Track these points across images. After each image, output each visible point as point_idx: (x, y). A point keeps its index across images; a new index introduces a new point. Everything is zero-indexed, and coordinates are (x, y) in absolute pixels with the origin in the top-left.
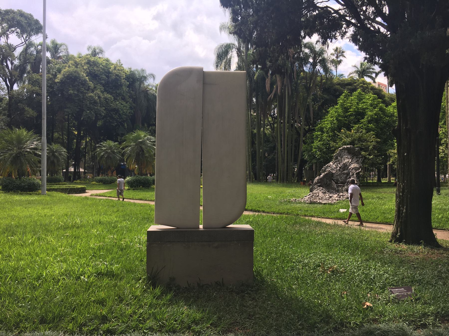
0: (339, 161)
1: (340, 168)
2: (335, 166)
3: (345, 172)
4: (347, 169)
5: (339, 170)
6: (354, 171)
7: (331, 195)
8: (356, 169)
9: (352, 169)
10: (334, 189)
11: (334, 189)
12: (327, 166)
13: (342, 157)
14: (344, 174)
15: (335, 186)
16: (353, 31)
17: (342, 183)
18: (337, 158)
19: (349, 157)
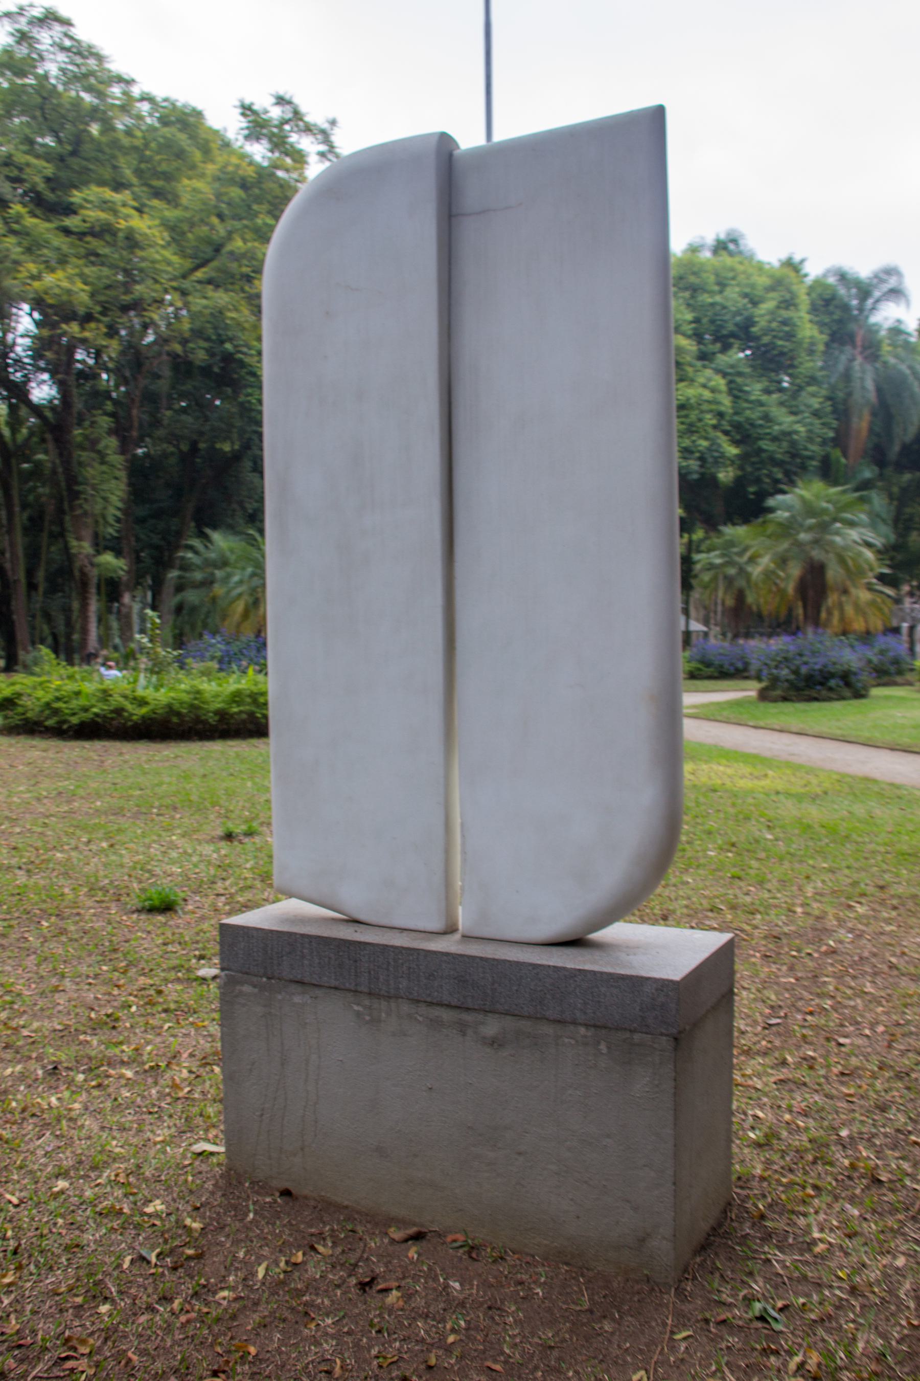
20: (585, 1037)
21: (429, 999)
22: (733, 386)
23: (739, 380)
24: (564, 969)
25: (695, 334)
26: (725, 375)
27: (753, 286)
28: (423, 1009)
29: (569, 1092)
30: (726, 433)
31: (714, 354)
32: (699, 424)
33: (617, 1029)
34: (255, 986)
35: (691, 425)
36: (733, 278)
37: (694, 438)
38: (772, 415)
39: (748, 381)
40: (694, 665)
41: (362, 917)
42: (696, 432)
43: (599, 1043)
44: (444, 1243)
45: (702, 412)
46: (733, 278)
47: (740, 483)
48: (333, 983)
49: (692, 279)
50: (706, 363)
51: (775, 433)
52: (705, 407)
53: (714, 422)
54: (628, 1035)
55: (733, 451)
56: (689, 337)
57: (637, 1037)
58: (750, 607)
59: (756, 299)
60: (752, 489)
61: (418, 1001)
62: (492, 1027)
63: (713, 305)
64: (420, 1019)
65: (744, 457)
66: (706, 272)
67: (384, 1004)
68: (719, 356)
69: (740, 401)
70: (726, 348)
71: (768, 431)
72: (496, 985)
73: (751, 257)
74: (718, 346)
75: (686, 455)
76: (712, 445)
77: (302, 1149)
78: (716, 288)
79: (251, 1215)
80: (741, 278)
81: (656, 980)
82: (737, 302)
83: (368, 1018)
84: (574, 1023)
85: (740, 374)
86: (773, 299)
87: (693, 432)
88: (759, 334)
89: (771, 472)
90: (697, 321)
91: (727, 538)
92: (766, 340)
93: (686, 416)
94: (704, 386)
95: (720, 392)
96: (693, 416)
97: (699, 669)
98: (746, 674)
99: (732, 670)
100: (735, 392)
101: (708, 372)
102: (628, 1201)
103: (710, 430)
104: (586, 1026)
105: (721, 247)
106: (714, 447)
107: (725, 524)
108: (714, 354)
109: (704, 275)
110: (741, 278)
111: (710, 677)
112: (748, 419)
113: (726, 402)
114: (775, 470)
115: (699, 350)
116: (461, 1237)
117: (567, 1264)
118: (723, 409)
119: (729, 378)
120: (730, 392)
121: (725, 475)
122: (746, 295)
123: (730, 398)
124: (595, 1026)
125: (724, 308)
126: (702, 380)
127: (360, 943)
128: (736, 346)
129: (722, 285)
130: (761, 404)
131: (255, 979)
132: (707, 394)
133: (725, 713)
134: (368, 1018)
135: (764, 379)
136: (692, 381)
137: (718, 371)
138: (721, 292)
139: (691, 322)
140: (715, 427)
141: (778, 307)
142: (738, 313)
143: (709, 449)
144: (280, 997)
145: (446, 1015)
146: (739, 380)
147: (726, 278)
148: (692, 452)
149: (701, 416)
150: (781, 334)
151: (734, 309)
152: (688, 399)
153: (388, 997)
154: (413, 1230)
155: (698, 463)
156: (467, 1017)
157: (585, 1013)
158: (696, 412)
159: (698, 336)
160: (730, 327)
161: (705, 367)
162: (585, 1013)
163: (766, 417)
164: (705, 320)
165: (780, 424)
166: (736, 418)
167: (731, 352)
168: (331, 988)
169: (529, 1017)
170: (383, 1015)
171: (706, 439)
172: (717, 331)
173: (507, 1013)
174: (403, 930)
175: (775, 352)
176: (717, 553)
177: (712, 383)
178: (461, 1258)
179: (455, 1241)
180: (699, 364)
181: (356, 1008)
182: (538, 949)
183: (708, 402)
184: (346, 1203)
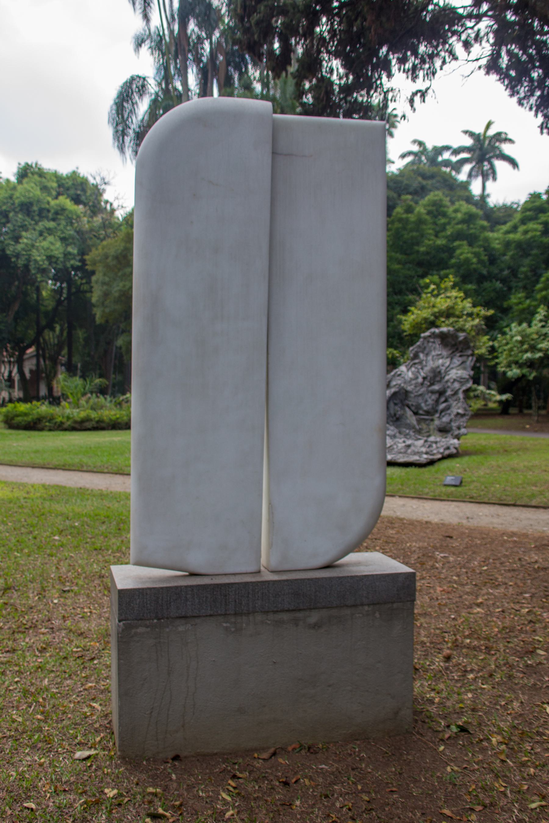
0: (420, 363)
1: (424, 378)
2: (413, 373)
3: (436, 387)
4: (440, 381)
5: (422, 384)
6: (456, 385)
7: (409, 442)
8: (461, 381)
9: (453, 383)
10: (410, 427)
11: (410, 427)
12: (394, 376)
13: (427, 355)
14: (433, 392)
15: (412, 419)
16: (67, 198)
17: (428, 413)
18: (416, 356)
19: (445, 353)
21: (275, 609)
28: (271, 616)
34: (147, 627)
48: (209, 612)
57: (395, 605)
61: (268, 612)
62: (314, 617)
64: (269, 622)
67: (244, 618)
77: (183, 726)
84: (362, 605)
104: (369, 605)
117: (357, 740)
134: (233, 629)
144: (167, 630)
145: (285, 616)
154: (272, 750)
168: (207, 616)
169: (337, 607)
179: (294, 749)
181: (225, 625)
182: (320, 571)
184: (215, 751)
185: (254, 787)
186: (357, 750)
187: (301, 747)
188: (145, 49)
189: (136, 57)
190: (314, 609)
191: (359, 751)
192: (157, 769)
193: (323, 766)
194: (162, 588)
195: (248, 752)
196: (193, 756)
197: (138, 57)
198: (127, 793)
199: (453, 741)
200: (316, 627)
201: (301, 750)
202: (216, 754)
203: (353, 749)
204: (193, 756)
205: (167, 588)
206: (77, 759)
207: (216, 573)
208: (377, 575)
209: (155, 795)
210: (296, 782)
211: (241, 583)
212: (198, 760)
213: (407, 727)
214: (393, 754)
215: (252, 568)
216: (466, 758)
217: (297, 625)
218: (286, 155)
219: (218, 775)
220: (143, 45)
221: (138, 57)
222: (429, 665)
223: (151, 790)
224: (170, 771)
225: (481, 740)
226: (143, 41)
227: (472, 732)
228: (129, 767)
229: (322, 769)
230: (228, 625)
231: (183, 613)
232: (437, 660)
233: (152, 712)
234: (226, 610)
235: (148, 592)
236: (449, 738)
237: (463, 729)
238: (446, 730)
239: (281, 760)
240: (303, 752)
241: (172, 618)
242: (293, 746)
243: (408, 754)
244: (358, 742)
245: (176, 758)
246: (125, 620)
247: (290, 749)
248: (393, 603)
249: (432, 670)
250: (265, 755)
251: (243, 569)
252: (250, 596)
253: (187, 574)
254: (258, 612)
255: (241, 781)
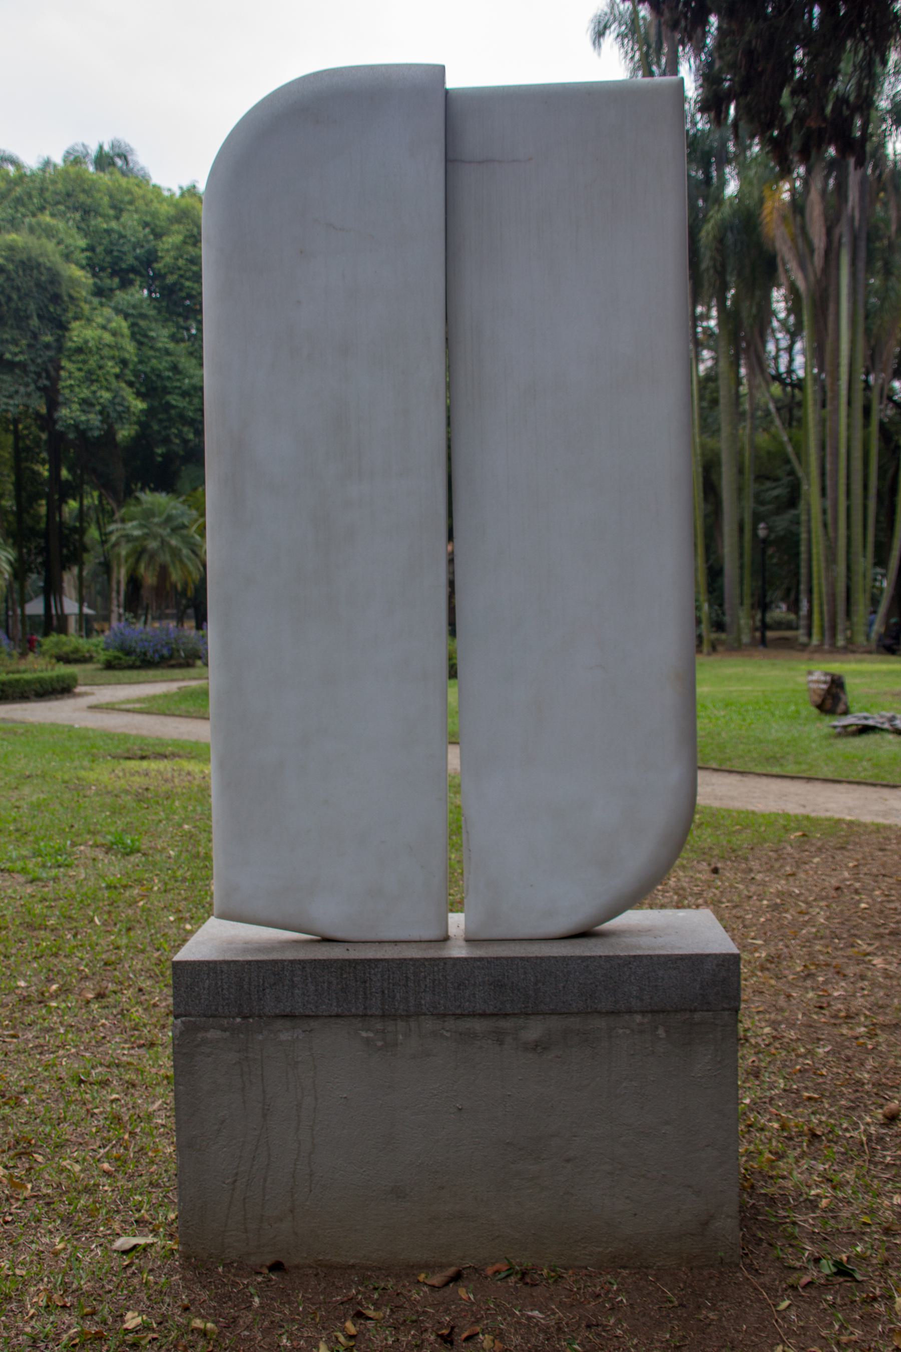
20: (641, 1024)
21: (459, 1011)
22: (136, 329)
23: (142, 323)
24: (618, 957)
25: (88, 265)
26: (126, 316)
27: (155, 215)
28: (451, 1023)
29: (624, 1084)
30: (130, 384)
31: (112, 290)
32: (100, 372)
33: (676, 1011)
34: (224, 1030)
35: (90, 372)
36: (131, 202)
37: (94, 388)
38: (181, 366)
39: (153, 325)
40: (112, 653)
41: (339, 935)
42: (97, 381)
43: (656, 1028)
44: (486, 1277)
45: (102, 358)
46: (131, 202)
47: (143, 440)
48: (335, 1010)
49: (82, 197)
50: (104, 300)
51: (185, 387)
52: (106, 352)
53: (117, 370)
54: (687, 1015)
55: (139, 405)
56: (82, 268)
57: (697, 1016)
58: (174, 586)
59: (158, 230)
60: (159, 451)
61: (445, 1015)
62: (534, 1030)
63: (108, 232)
64: (448, 1035)
65: (150, 412)
66: (99, 191)
67: (401, 1025)
68: (118, 292)
69: (145, 349)
70: (125, 284)
71: (178, 384)
72: (540, 985)
73: (143, 180)
74: (116, 280)
75: (85, 407)
76: (115, 397)
77: (291, 1211)
78: (112, 212)
79: (257, 1300)
80: (140, 203)
81: (716, 956)
82: (135, 231)
83: (380, 1044)
84: (630, 1012)
85: (143, 316)
86: (178, 232)
87: (92, 382)
88: (163, 272)
89: (180, 431)
90: (91, 248)
91: (145, 506)
92: (171, 279)
93: (84, 362)
94: (104, 328)
95: (123, 336)
96: (92, 363)
97: (119, 658)
98: (173, 662)
99: (157, 658)
100: (140, 337)
101: (108, 311)
102: (689, 1186)
103: (113, 380)
104: (643, 1013)
105: (104, 161)
106: (118, 400)
107: (142, 489)
108: (112, 290)
109: (98, 195)
110: (140, 203)
111: (132, 667)
112: (153, 370)
113: (130, 347)
114: (186, 429)
115: (95, 284)
116: (502, 1266)
117: (625, 1267)
118: (127, 356)
119: (131, 320)
120: (133, 335)
121: (124, 433)
122: (146, 225)
123: (133, 344)
124: (653, 1012)
125: (122, 236)
126: (100, 320)
127: (370, 960)
128: (138, 283)
129: (118, 210)
130: (168, 352)
131: (225, 1022)
132: (108, 338)
133: (183, 706)
134: (380, 1044)
135: (170, 324)
136: (89, 320)
137: (118, 311)
138: (117, 218)
139: (83, 250)
140: (117, 377)
141: (184, 242)
142: (138, 244)
143: (112, 402)
144: (260, 1037)
145: (479, 1025)
146: (142, 323)
147: (122, 202)
148: (92, 405)
149: (101, 362)
150: (189, 274)
151: (133, 239)
152: (86, 342)
153: (407, 1017)
154: (451, 1271)
155: (100, 418)
156: (504, 1024)
157: (642, 1000)
158: (96, 357)
159: (91, 266)
160: (130, 260)
161: (102, 304)
162: (642, 1000)
163: (175, 368)
164: (99, 249)
165: (190, 377)
166: (140, 367)
167: (132, 290)
168: (330, 1016)
169: (578, 1013)
170: (401, 1037)
171: (108, 389)
172: (116, 264)
173: (553, 1013)
174: (396, 942)
175: (183, 294)
176: (135, 523)
177: (114, 325)
178: (516, 1288)
179: (498, 1272)
180: (96, 301)
181: (364, 1034)
182: (556, 944)
183: (109, 346)
184: (352, 1262)
185: (386, 1339)
186: (615, 1287)
187: (511, 1271)
188: (609, 39)
189: (595, 54)
190: (533, 1014)
191: (619, 1290)
192: (234, 1284)
193: (536, 1313)
194: (249, 963)
195: (410, 1270)
196: (311, 1267)
197: (599, 54)
198: (160, 1324)
199: (814, 1293)
200: (539, 1049)
201: (508, 1276)
202: (353, 1266)
203: (608, 1285)
204: (311, 1267)
205: (257, 962)
206: (115, 1251)
207: (363, 939)
208: (659, 956)
209: (204, 1333)
210: (468, 1339)
211: (393, 960)
212: (316, 1275)
213: (721, 1254)
214: (682, 1305)
215: (432, 933)
216: (824, 1333)
217: (501, 1043)
218: (479, 163)
219: (335, 1308)
220: (607, 32)
221: (599, 54)
222: (846, 1130)
223: (198, 1323)
224: (253, 1291)
225: (874, 1299)
226: (606, 27)
227: (859, 1277)
228: (189, 1274)
229: (530, 1318)
230: (371, 1035)
231: (288, 1010)
232: (868, 1119)
233: (235, 1181)
234: (365, 1008)
235: (225, 967)
236: (810, 1283)
237: (842, 1271)
238: (811, 1266)
239: (462, 1292)
240: (512, 1279)
241: (269, 1017)
242: (498, 1266)
243: (714, 1308)
244: (625, 1272)
245: (277, 1267)
246: (185, 1016)
247: (490, 1271)
248: (693, 1011)
249: (847, 1139)
250: (437, 1280)
251: (415, 935)
252: (411, 984)
253: (319, 938)
254: (425, 1014)
255: (370, 1324)
